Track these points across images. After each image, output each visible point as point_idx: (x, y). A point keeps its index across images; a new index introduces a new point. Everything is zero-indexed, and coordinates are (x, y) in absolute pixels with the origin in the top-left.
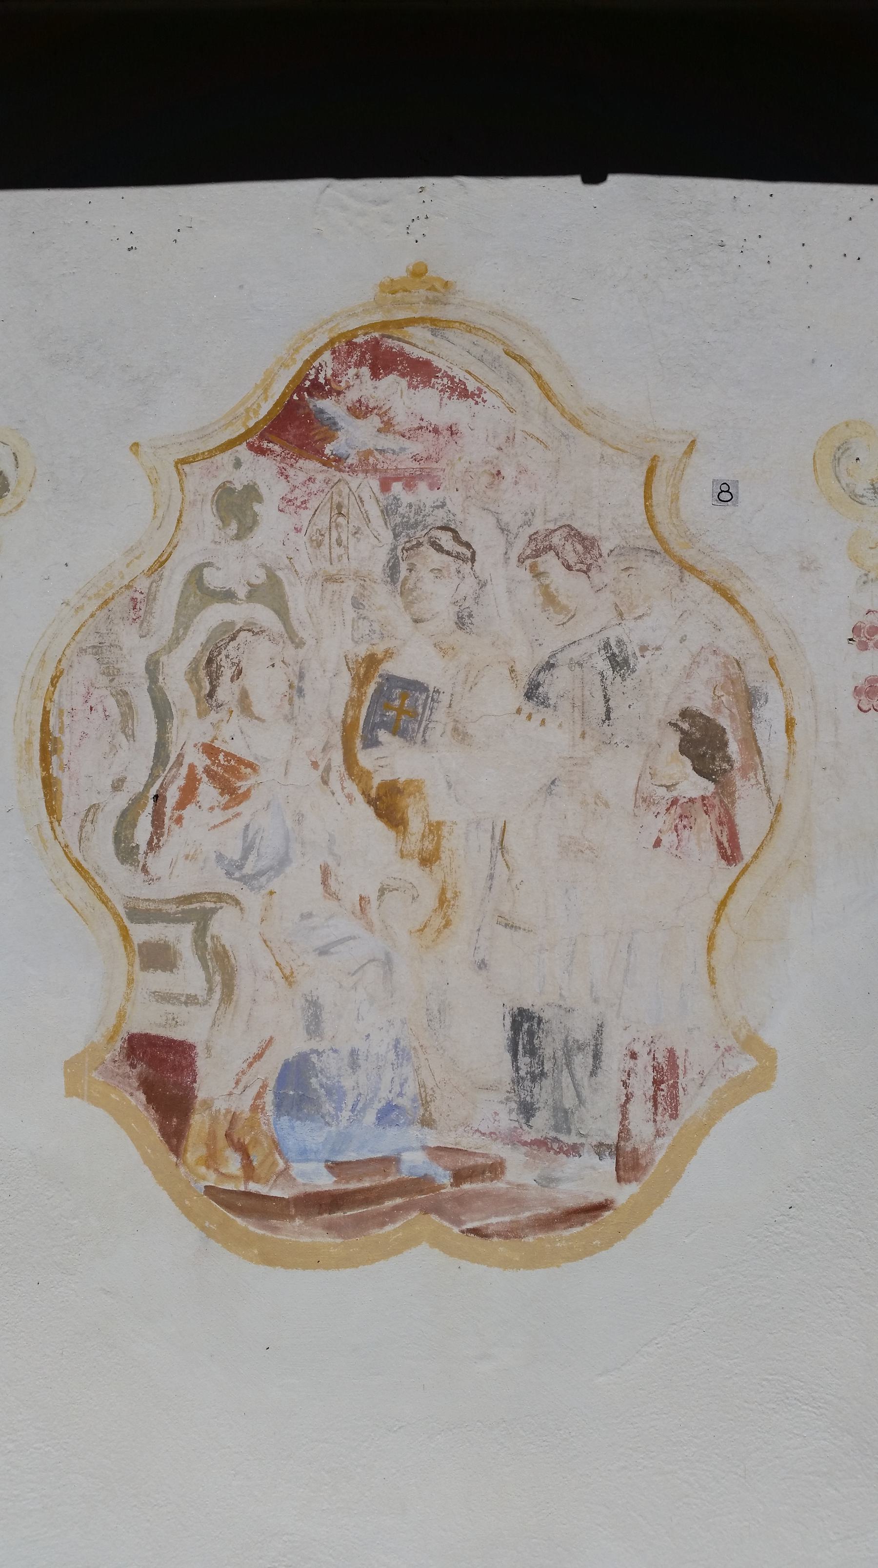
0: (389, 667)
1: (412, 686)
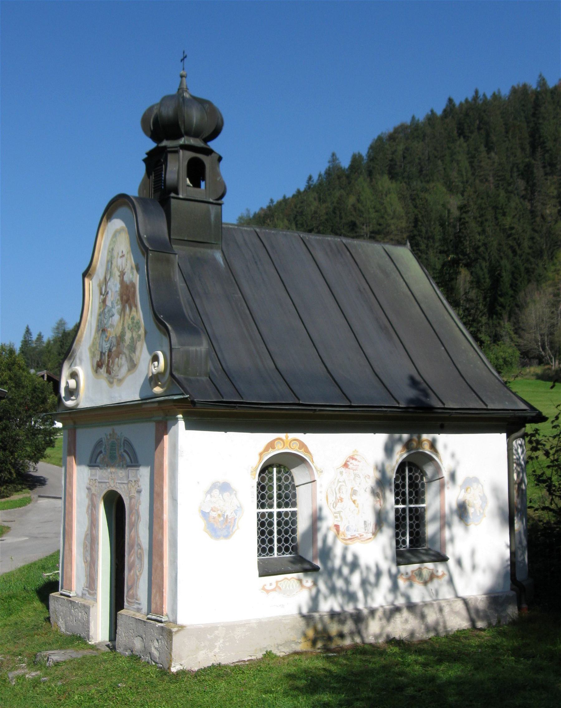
0: (354, 489)
1: (356, 490)
